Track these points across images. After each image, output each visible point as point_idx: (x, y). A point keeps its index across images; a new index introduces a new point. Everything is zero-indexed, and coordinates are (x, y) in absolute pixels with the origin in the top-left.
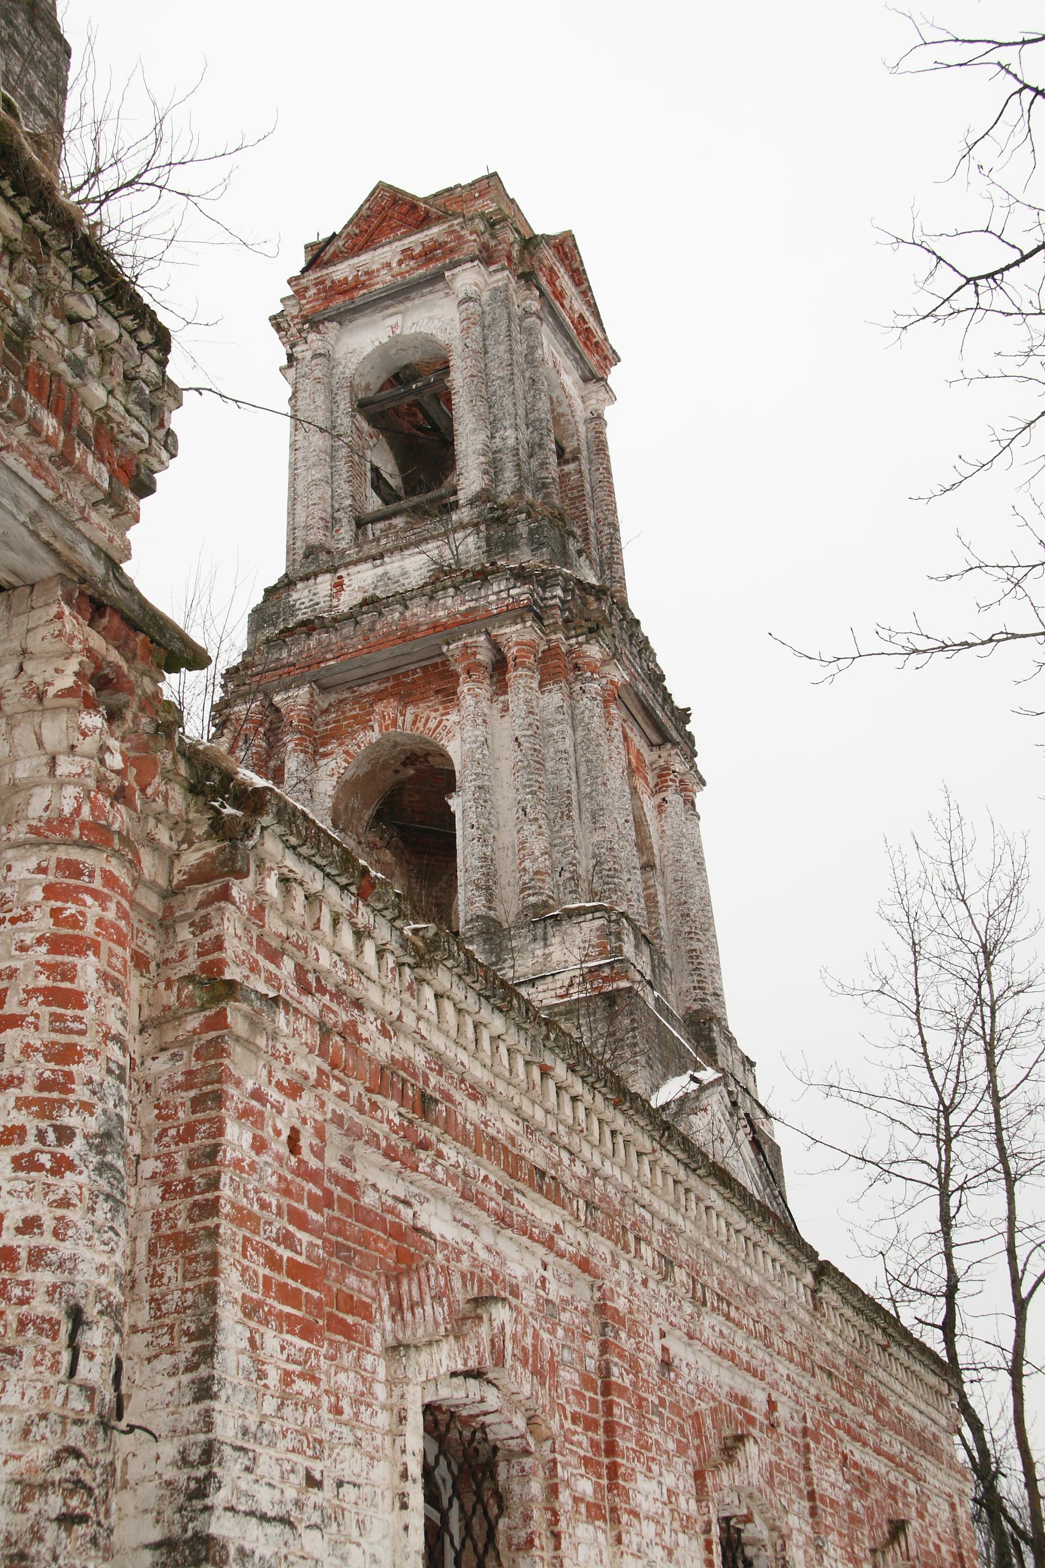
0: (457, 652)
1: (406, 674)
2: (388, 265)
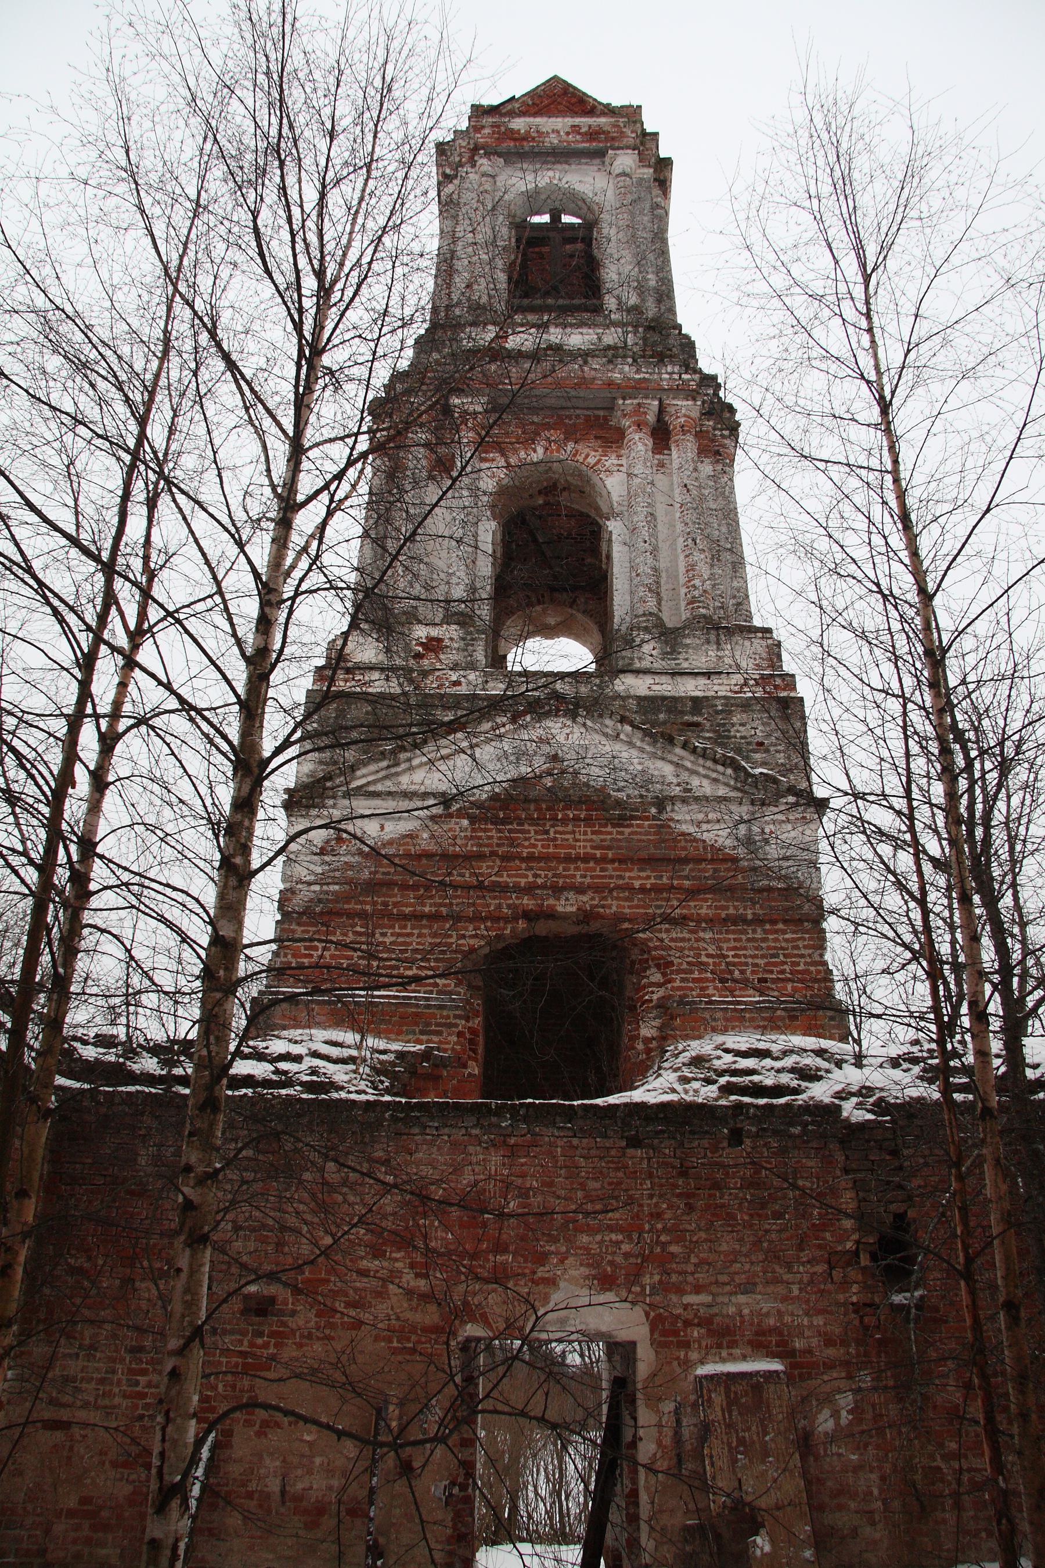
0: (630, 408)
1: (570, 417)
2: (558, 132)
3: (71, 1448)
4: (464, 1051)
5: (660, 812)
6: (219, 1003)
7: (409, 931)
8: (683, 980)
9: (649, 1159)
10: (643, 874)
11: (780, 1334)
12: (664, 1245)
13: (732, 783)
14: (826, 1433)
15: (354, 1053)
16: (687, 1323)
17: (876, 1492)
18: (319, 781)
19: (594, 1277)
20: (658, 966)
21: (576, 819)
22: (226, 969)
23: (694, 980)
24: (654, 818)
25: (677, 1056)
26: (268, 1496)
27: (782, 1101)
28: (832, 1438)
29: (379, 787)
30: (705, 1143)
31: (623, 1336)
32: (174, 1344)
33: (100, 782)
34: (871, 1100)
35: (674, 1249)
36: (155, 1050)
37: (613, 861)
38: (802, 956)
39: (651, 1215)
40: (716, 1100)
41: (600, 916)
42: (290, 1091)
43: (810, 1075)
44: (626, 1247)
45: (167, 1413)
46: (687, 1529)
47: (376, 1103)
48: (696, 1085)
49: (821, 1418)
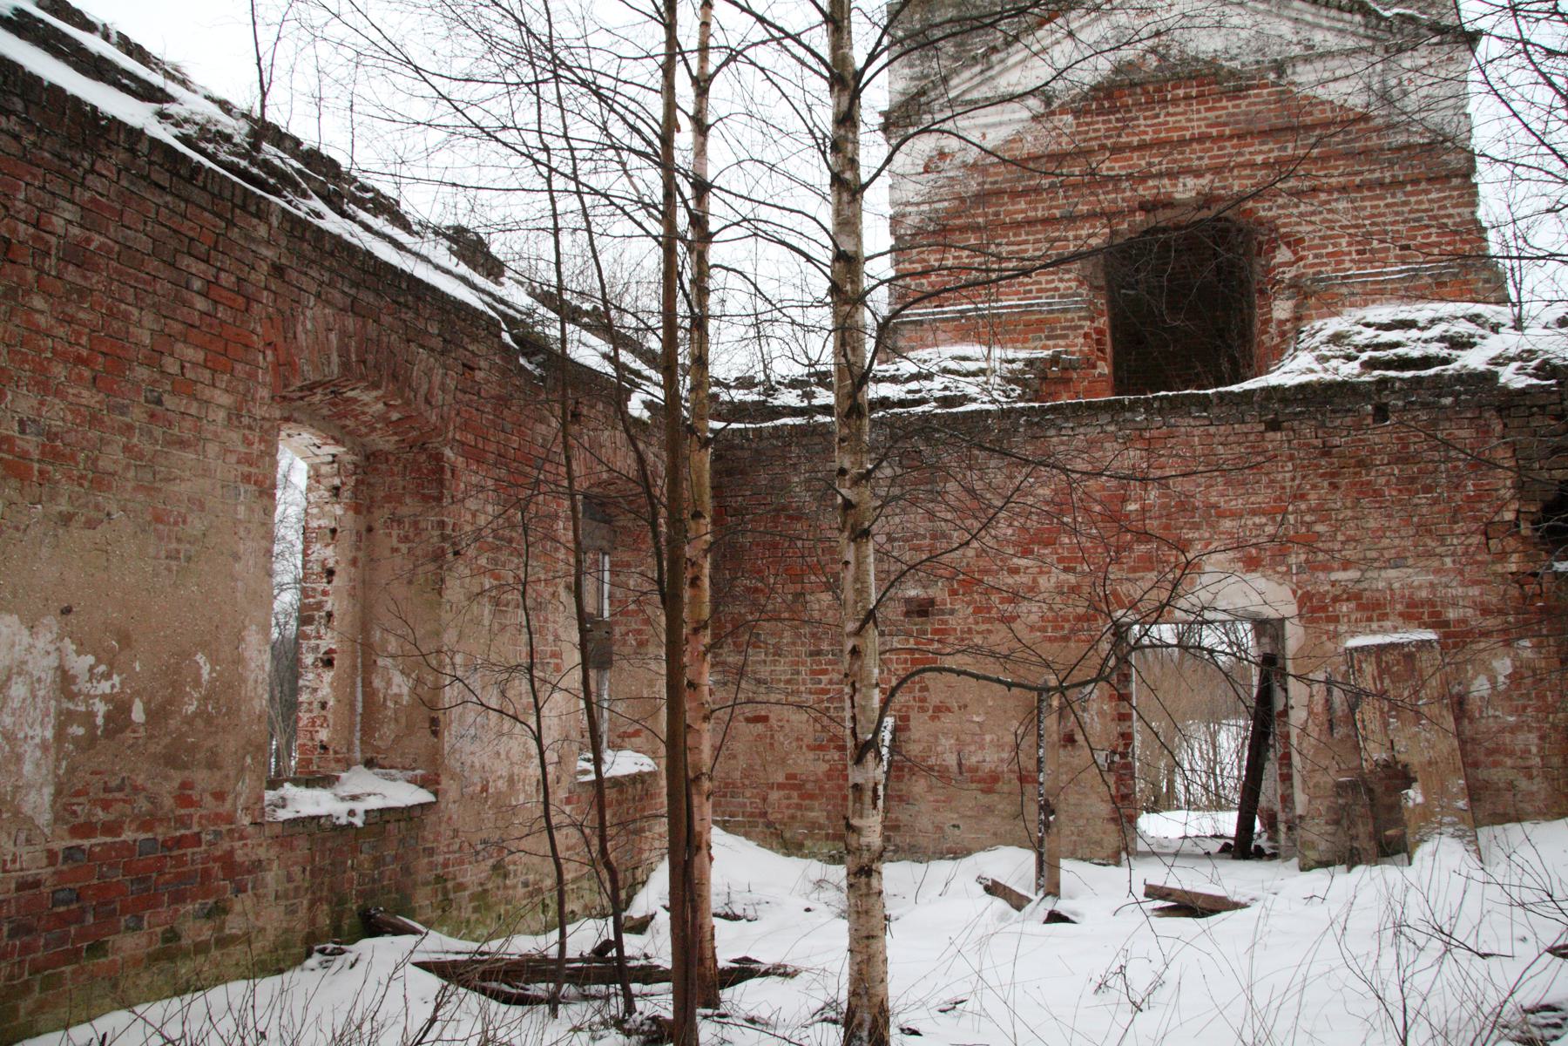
3: (772, 737)
4: (1092, 352)
5: (1280, 77)
6: (849, 315)
7: (1024, 237)
8: (1316, 256)
9: (1289, 442)
10: (1265, 148)
11: (1433, 605)
12: (1309, 525)
13: (1361, 30)
14: (1482, 698)
15: (984, 365)
16: (1336, 599)
17: (1534, 750)
18: (913, 98)
19: (1239, 560)
20: (1288, 245)
21: (1187, 97)
22: (852, 282)
23: (1329, 255)
24: (1274, 84)
25: (1313, 336)
26: (947, 768)
27: (1432, 371)
28: (1488, 702)
29: (975, 95)
30: (1348, 420)
31: (1269, 613)
32: (851, 626)
33: (701, 128)
34: (1534, 364)
35: (1320, 528)
36: (794, 384)
37: (1231, 137)
38: (1450, 216)
39: (1295, 497)
40: (1358, 376)
41: (1220, 198)
42: (926, 408)
43: (1460, 343)
44: (1270, 529)
45: (853, 684)
46: (1339, 785)
47: (1011, 410)
48: (1334, 363)
49: (1477, 683)
